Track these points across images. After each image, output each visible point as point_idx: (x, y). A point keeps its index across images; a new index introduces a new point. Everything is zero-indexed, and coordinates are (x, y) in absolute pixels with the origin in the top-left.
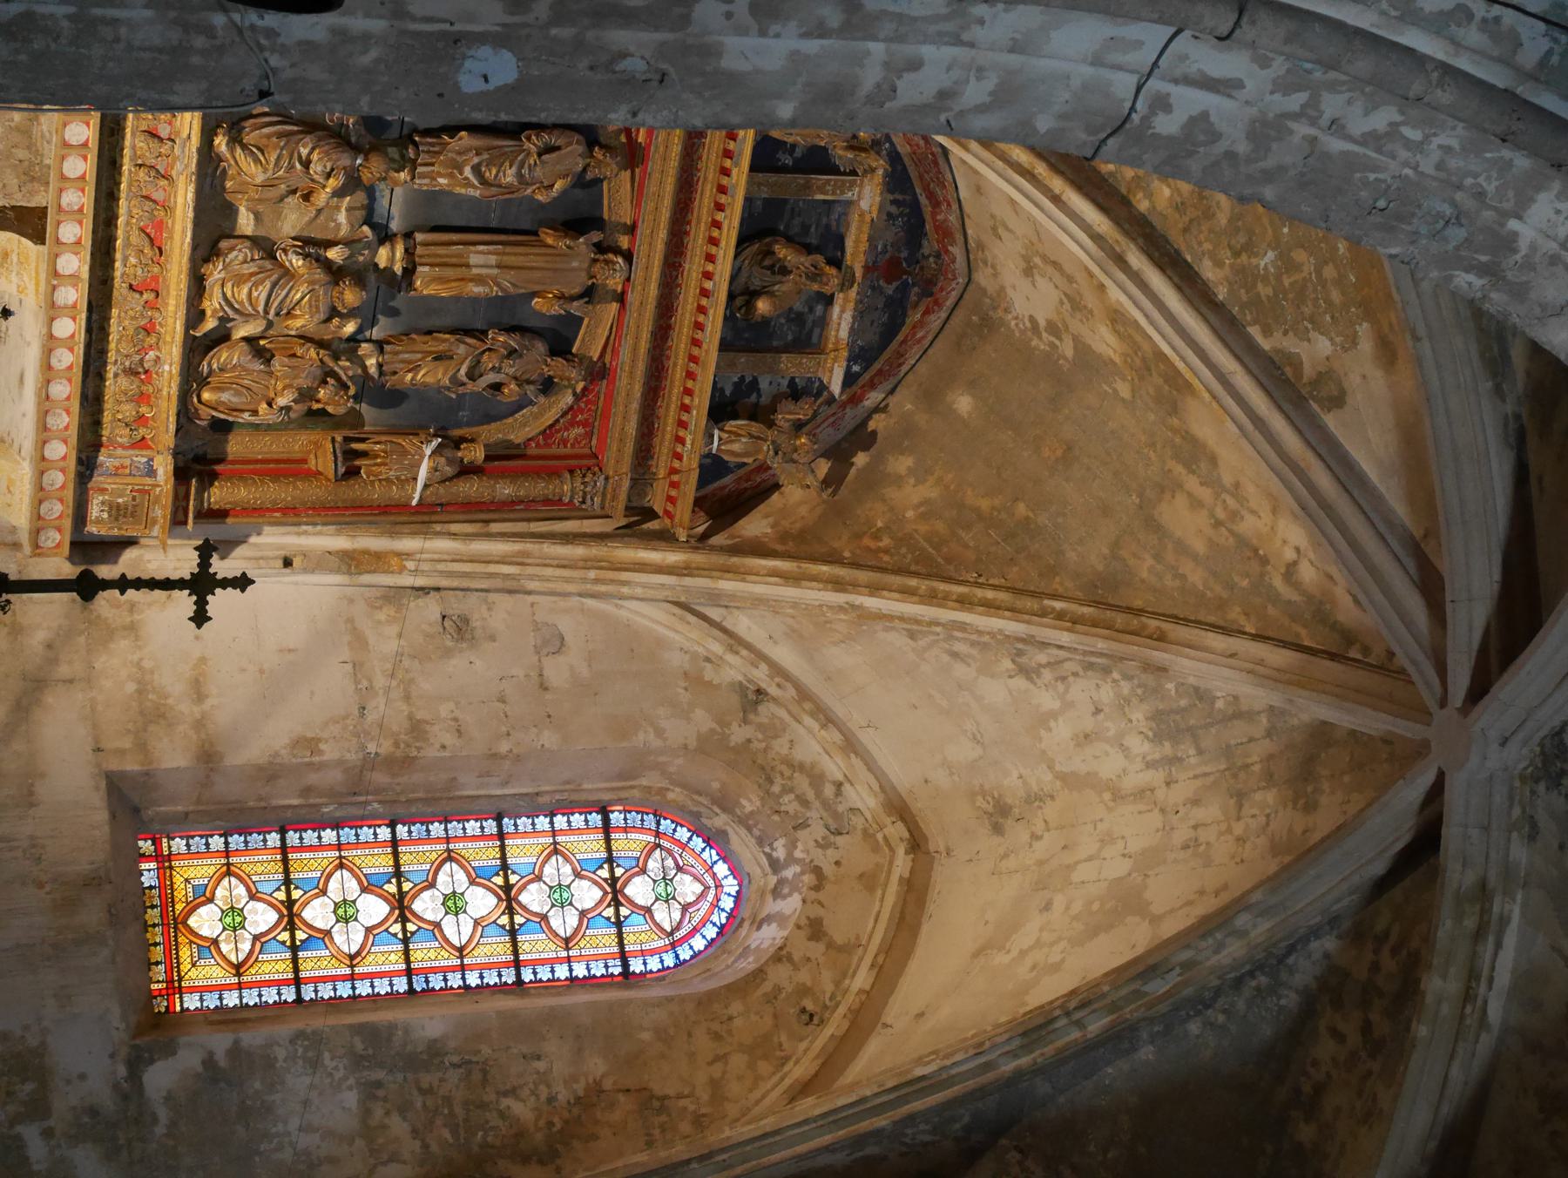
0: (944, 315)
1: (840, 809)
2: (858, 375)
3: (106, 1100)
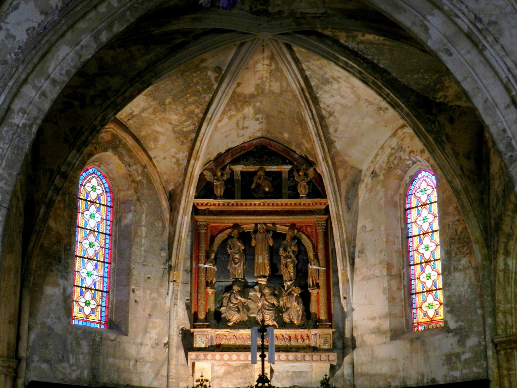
0: (272, 142)
1: (397, 148)
2: (289, 160)
3: (456, 338)
